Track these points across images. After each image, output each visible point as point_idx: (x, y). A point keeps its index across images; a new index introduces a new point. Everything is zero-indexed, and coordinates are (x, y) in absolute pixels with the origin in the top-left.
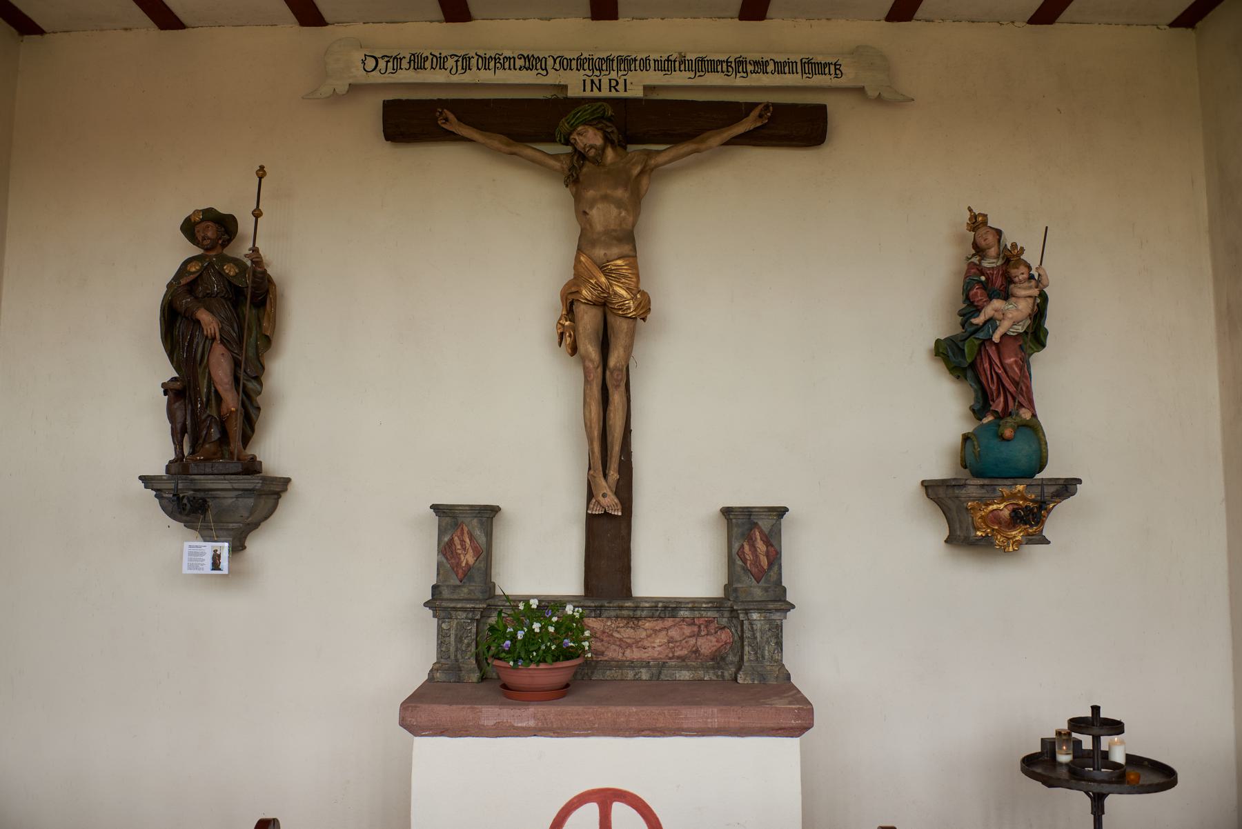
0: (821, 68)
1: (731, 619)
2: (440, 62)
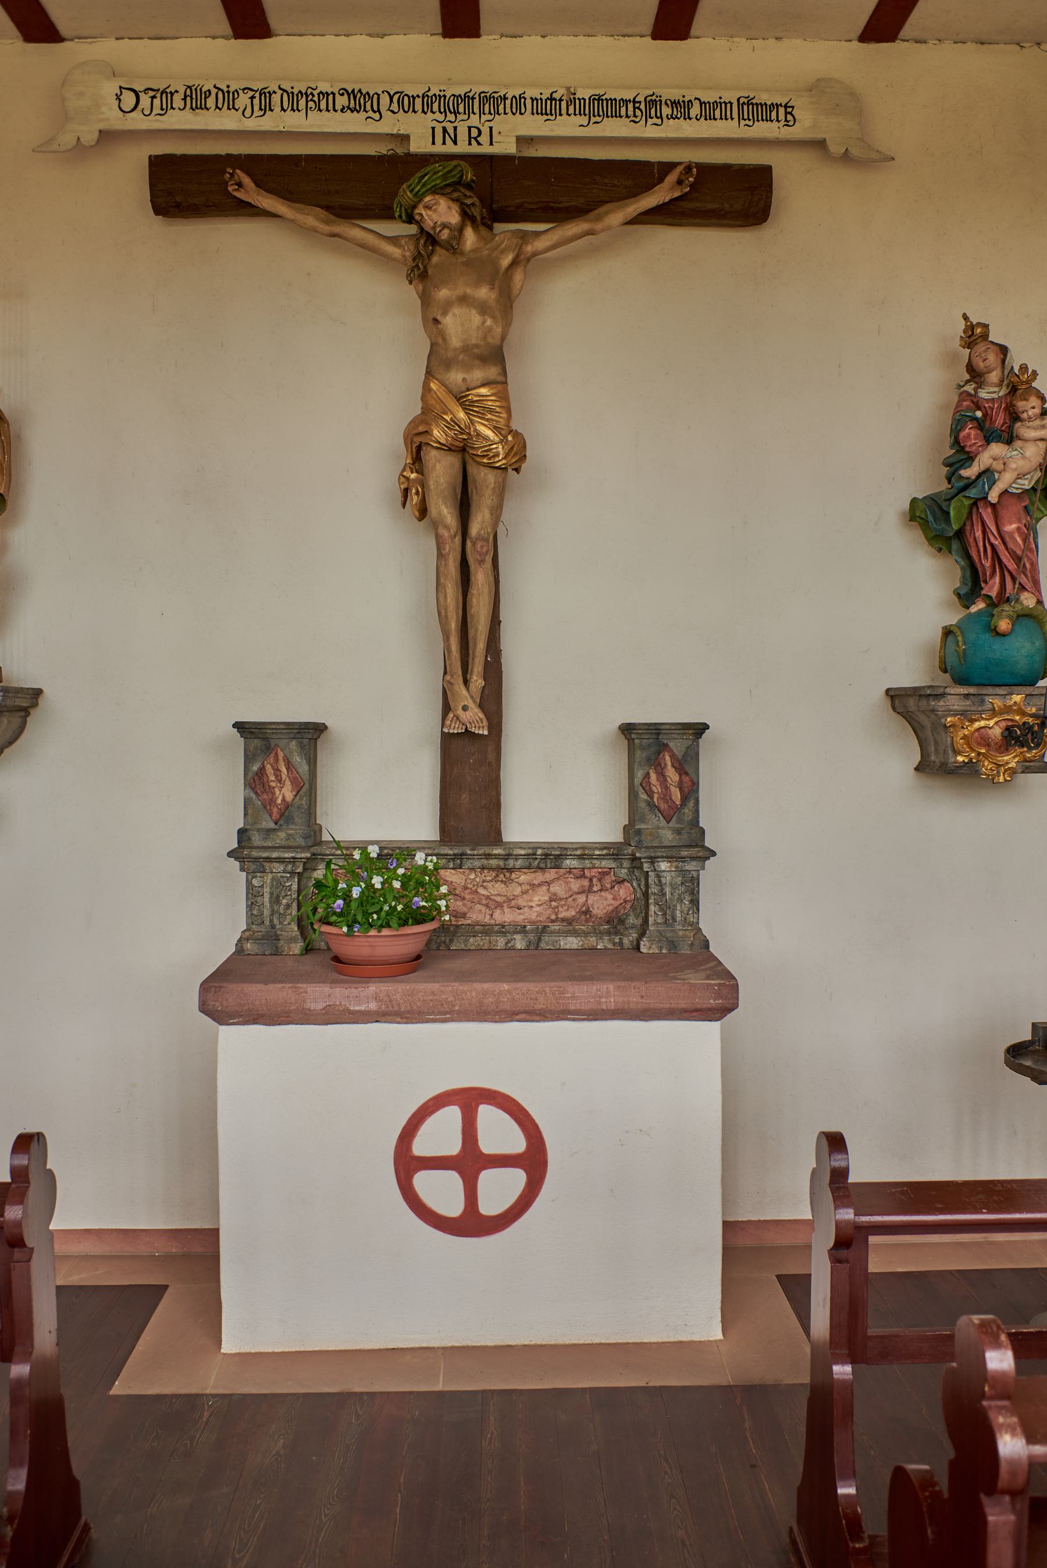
0: (763, 111)
1: (631, 870)
2: (228, 98)
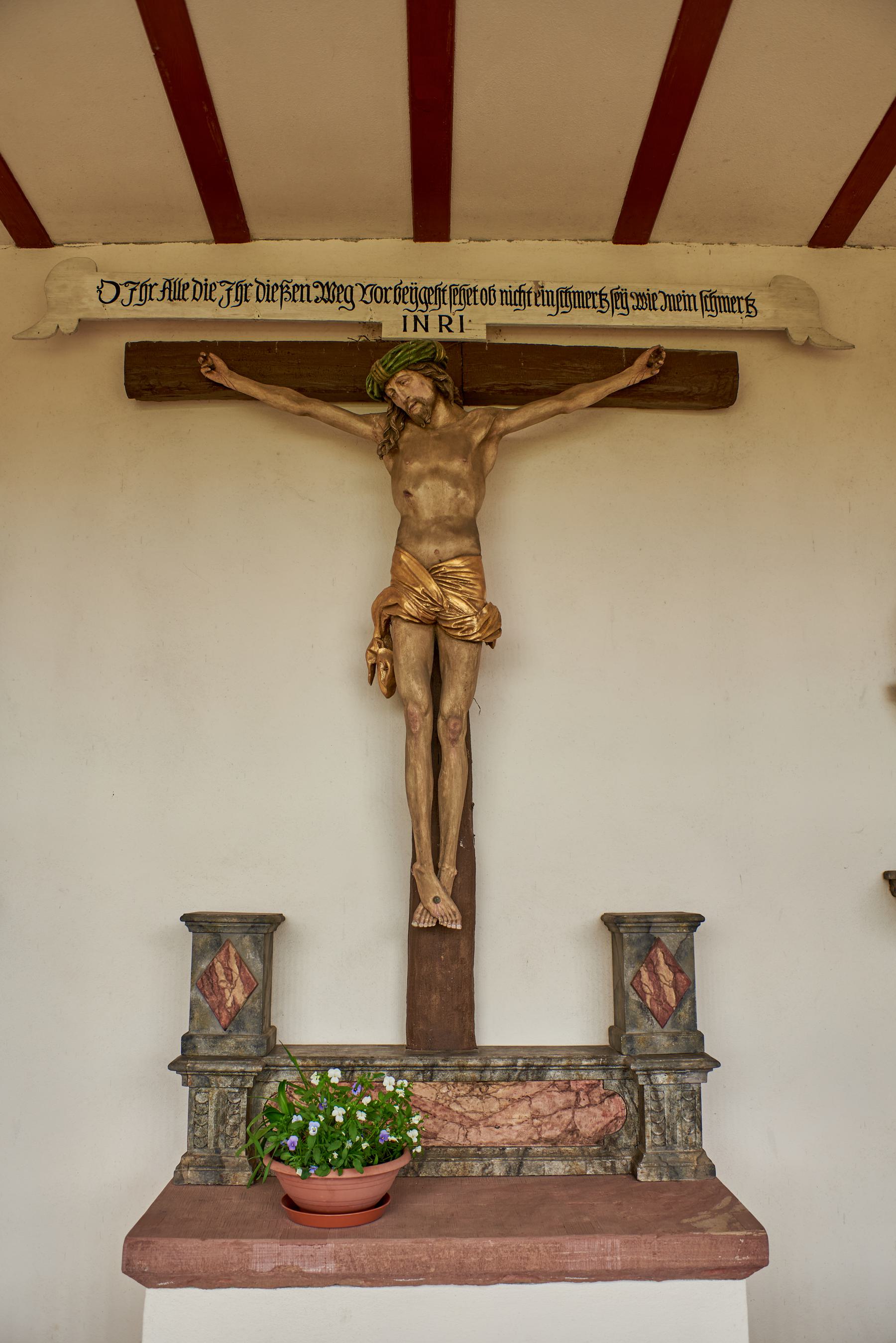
0: (728, 304)
1: (623, 1082)
2: (206, 290)
